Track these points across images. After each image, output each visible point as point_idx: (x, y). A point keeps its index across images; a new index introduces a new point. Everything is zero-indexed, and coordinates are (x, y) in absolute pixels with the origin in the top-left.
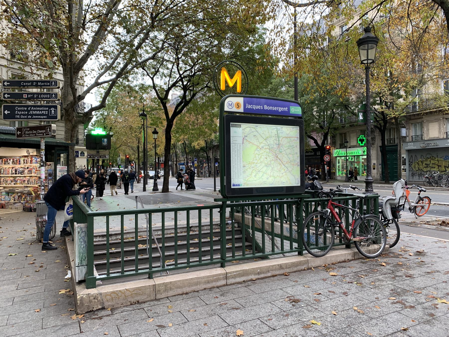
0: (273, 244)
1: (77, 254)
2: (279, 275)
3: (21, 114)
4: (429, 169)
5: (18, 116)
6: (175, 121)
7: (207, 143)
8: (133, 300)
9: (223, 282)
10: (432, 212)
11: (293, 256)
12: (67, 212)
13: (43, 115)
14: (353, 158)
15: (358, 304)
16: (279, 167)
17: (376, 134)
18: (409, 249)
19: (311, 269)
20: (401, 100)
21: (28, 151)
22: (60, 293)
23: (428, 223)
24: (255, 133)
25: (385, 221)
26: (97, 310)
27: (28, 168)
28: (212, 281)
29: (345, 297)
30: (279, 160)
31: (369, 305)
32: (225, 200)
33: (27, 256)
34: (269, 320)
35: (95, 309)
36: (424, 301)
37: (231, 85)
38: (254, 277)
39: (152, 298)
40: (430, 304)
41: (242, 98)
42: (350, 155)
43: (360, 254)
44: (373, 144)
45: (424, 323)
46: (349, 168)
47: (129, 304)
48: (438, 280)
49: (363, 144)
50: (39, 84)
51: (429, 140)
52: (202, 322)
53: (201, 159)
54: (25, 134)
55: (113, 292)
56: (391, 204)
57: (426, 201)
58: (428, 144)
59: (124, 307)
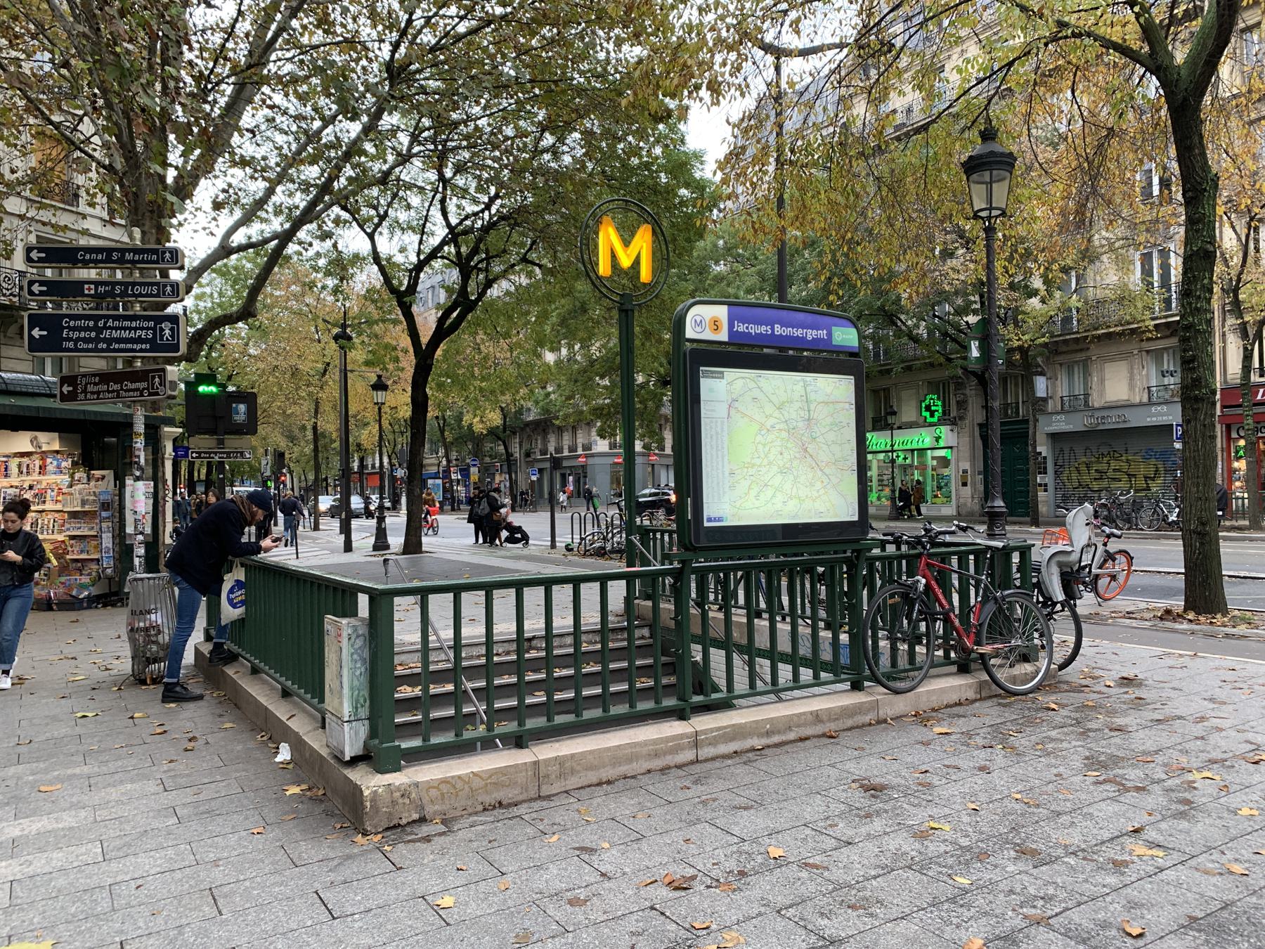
0: (753, 676)
1: (346, 691)
2: (814, 737)
3: (79, 339)
4: (1105, 484)
5: (71, 345)
6: (439, 352)
7: (505, 418)
8: (488, 799)
9: (689, 755)
10: (1134, 592)
11: (836, 692)
12: (230, 601)
13: (139, 340)
14: (909, 455)
15: (1020, 788)
16: (811, 475)
17: (968, 392)
18: (1100, 673)
19: (885, 721)
20: (1034, 301)
21: (36, 438)
22: (288, 793)
23: (1129, 615)
24: (756, 393)
25: (1045, 605)
26: (409, 823)
27: (31, 487)
28: (666, 753)
29: (985, 776)
30: (809, 459)
31: (1044, 789)
32: (688, 555)
33: (132, 718)
34: (831, 826)
35: (404, 822)
36: (1164, 776)
37: (626, 262)
38: (757, 742)
39: (533, 794)
40: (1178, 781)
41: (725, 307)
42: (901, 447)
43: (994, 687)
44: (961, 418)
45: (1174, 816)
46: (898, 484)
47: (480, 808)
48: (1183, 735)
49: (935, 420)
50: (128, 256)
51: (1104, 408)
52: (678, 837)
53: (487, 460)
54: (85, 391)
55: (444, 781)
56: (1060, 565)
57: (1121, 559)
58: (1103, 418)
59: (470, 815)
